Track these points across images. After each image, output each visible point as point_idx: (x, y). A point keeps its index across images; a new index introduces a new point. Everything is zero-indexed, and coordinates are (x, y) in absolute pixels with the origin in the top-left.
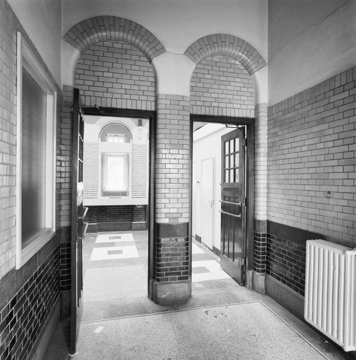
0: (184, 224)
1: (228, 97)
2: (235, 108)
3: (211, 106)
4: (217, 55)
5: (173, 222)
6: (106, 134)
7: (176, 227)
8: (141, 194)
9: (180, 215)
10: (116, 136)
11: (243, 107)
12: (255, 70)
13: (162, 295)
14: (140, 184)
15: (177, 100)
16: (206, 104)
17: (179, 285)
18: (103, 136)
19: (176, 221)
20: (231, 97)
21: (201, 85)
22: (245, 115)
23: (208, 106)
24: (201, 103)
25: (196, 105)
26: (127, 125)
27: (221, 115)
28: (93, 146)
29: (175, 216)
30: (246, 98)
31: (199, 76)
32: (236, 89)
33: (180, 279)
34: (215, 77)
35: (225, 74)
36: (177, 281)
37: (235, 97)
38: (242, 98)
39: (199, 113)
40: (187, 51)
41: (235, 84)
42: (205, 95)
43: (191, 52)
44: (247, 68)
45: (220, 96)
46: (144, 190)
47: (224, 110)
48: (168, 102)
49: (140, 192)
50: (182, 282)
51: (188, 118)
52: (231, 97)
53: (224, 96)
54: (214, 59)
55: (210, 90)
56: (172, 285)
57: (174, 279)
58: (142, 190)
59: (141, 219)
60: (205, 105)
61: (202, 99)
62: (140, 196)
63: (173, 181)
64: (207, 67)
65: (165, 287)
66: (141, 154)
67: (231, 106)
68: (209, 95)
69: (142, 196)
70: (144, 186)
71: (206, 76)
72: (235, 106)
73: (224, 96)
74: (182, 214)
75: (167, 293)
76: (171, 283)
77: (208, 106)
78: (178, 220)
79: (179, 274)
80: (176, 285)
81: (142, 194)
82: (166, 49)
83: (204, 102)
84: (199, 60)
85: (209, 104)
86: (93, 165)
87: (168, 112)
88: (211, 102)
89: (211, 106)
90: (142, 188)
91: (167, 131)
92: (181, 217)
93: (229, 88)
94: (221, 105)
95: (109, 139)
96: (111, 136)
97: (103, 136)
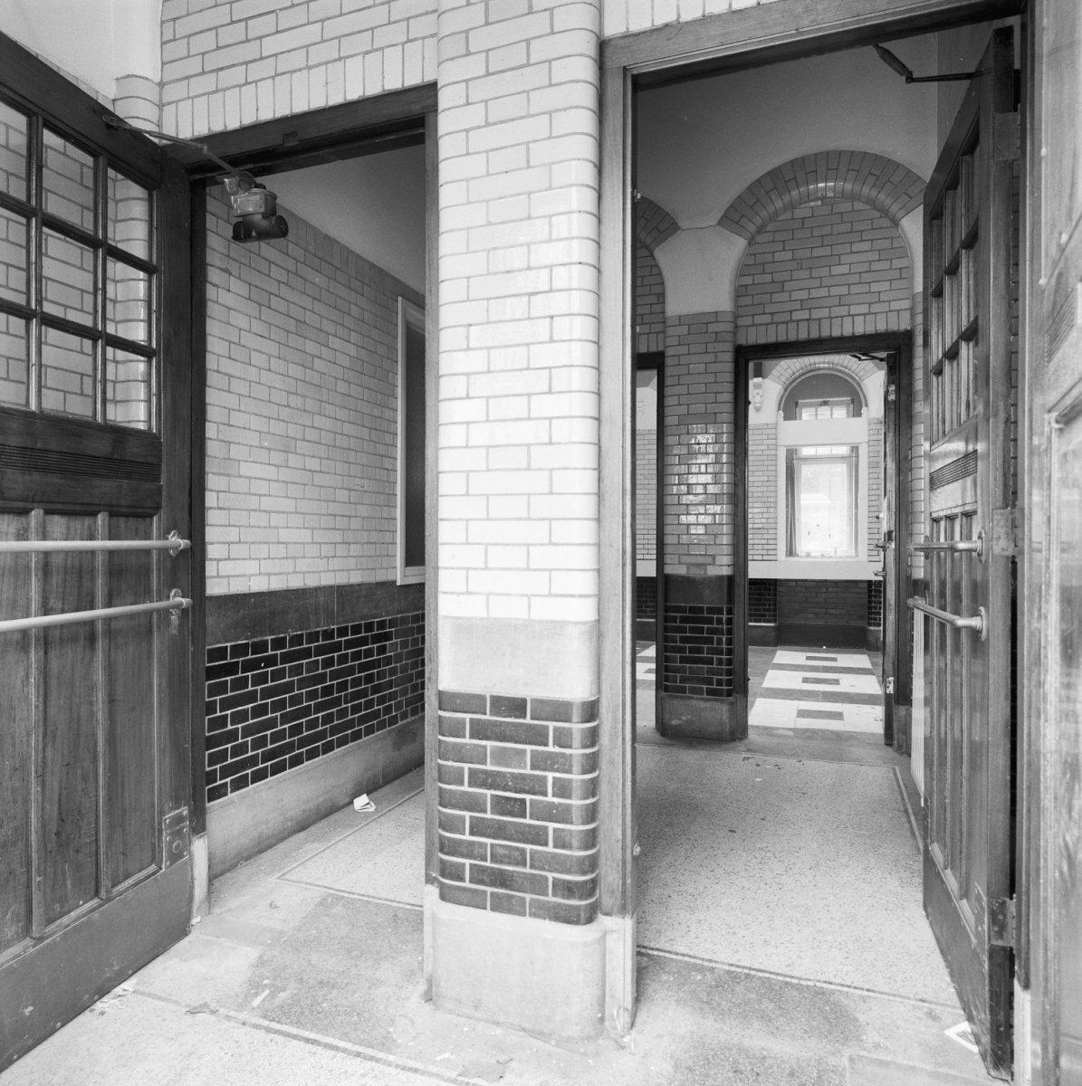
0: (721, 578)
1: (835, 291)
2: (853, 316)
3: (792, 321)
4: (805, 202)
5: (696, 573)
6: (797, 403)
7: (701, 583)
8: (761, 552)
9: (709, 560)
10: (825, 403)
11: (875, 308)
12: (901, 213)
13: (671, 719)
14: (760, 526)
15: (699, 323)
16: (777, 318)
17: (708, 704)
18: (790, 406)
19: (702, 572)
20: (844, 290)
21: (768, 278)
22: (881, 328)
23: (783, 323)
24: (766, 319)
25: (753, 325)
26: (853, 368)
27: (817, 336)
28: (646, 437)
29: (700, 560)
30: (886, 286)
31: (760, 259)
32: (855, 269)
33: (710, 692)
34: (800, 254)
35: (827, 241)
36: (705, 696)
37: (855, 289)
38: (875, 287)
39: (762, 341)
40: (724, 216)
41: (855, 258)
42: (777, 297)
43: (732, 219)
44: (885, 212)
45: (814, 293)
46: (771, 542)
47: (825, 324)
48: (684, 330)
49: (760, 547)
50: (715, 700)
51: (729, 357)
52: (844, 290)
53: (824, 292)
54: (799, 213)
55: (788, 286)
56: (694, 702)
57: (699, 691)
58: (764, 542)
59: (762, 615)
60: (775, 320)
61: (769, 309)
62: (760, 558)
63: (700, 489)
64: (779, 237)
65: (676, 703)
66: (763, 448)
67: (843, 311)
68: (785, 296)
69: (765, 558)
70: (771, 531)
71: (778, 256)
72: (854, 310)
73: (824, 292)
74: (714, 557)
75: (684, 718)
76: (692, 698)
77: (783, 323)
78: (706, 570)
79: (709, 682)
80: (703, 704)
81: (765, 552)
82: (680, 224)
83: (772, 314)
84: (752, 228)
85: (786, 317)
86: (646, 482)
87: (684, 350)
88: (791, 312)
89: (792, 321)
90: (765, 536)
91: (683, 390)
92: (713, 564)
93: (836, 270)
94: (816, 314)
95: (804, 415)
96: (811, 405)
97: (790, 406)
